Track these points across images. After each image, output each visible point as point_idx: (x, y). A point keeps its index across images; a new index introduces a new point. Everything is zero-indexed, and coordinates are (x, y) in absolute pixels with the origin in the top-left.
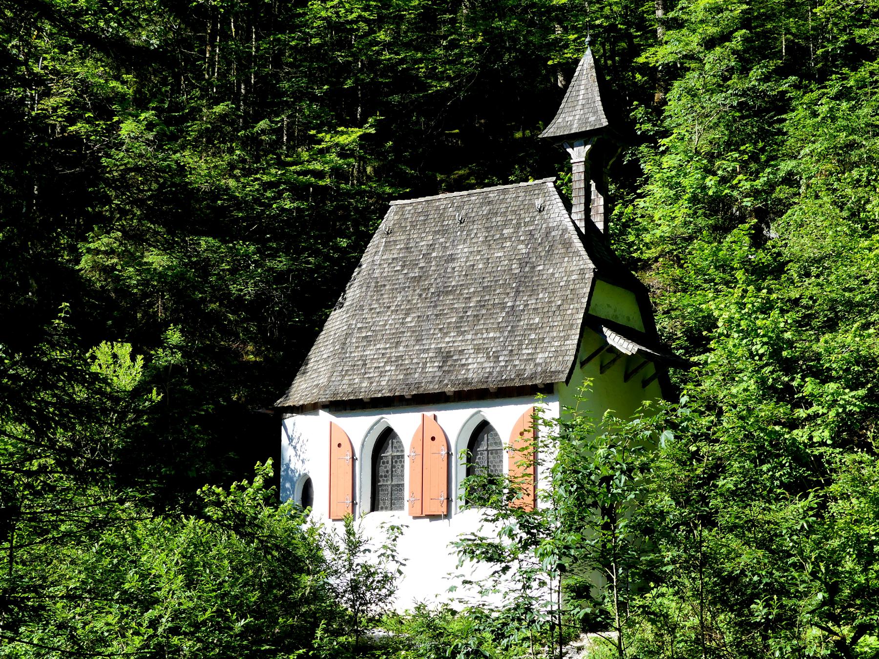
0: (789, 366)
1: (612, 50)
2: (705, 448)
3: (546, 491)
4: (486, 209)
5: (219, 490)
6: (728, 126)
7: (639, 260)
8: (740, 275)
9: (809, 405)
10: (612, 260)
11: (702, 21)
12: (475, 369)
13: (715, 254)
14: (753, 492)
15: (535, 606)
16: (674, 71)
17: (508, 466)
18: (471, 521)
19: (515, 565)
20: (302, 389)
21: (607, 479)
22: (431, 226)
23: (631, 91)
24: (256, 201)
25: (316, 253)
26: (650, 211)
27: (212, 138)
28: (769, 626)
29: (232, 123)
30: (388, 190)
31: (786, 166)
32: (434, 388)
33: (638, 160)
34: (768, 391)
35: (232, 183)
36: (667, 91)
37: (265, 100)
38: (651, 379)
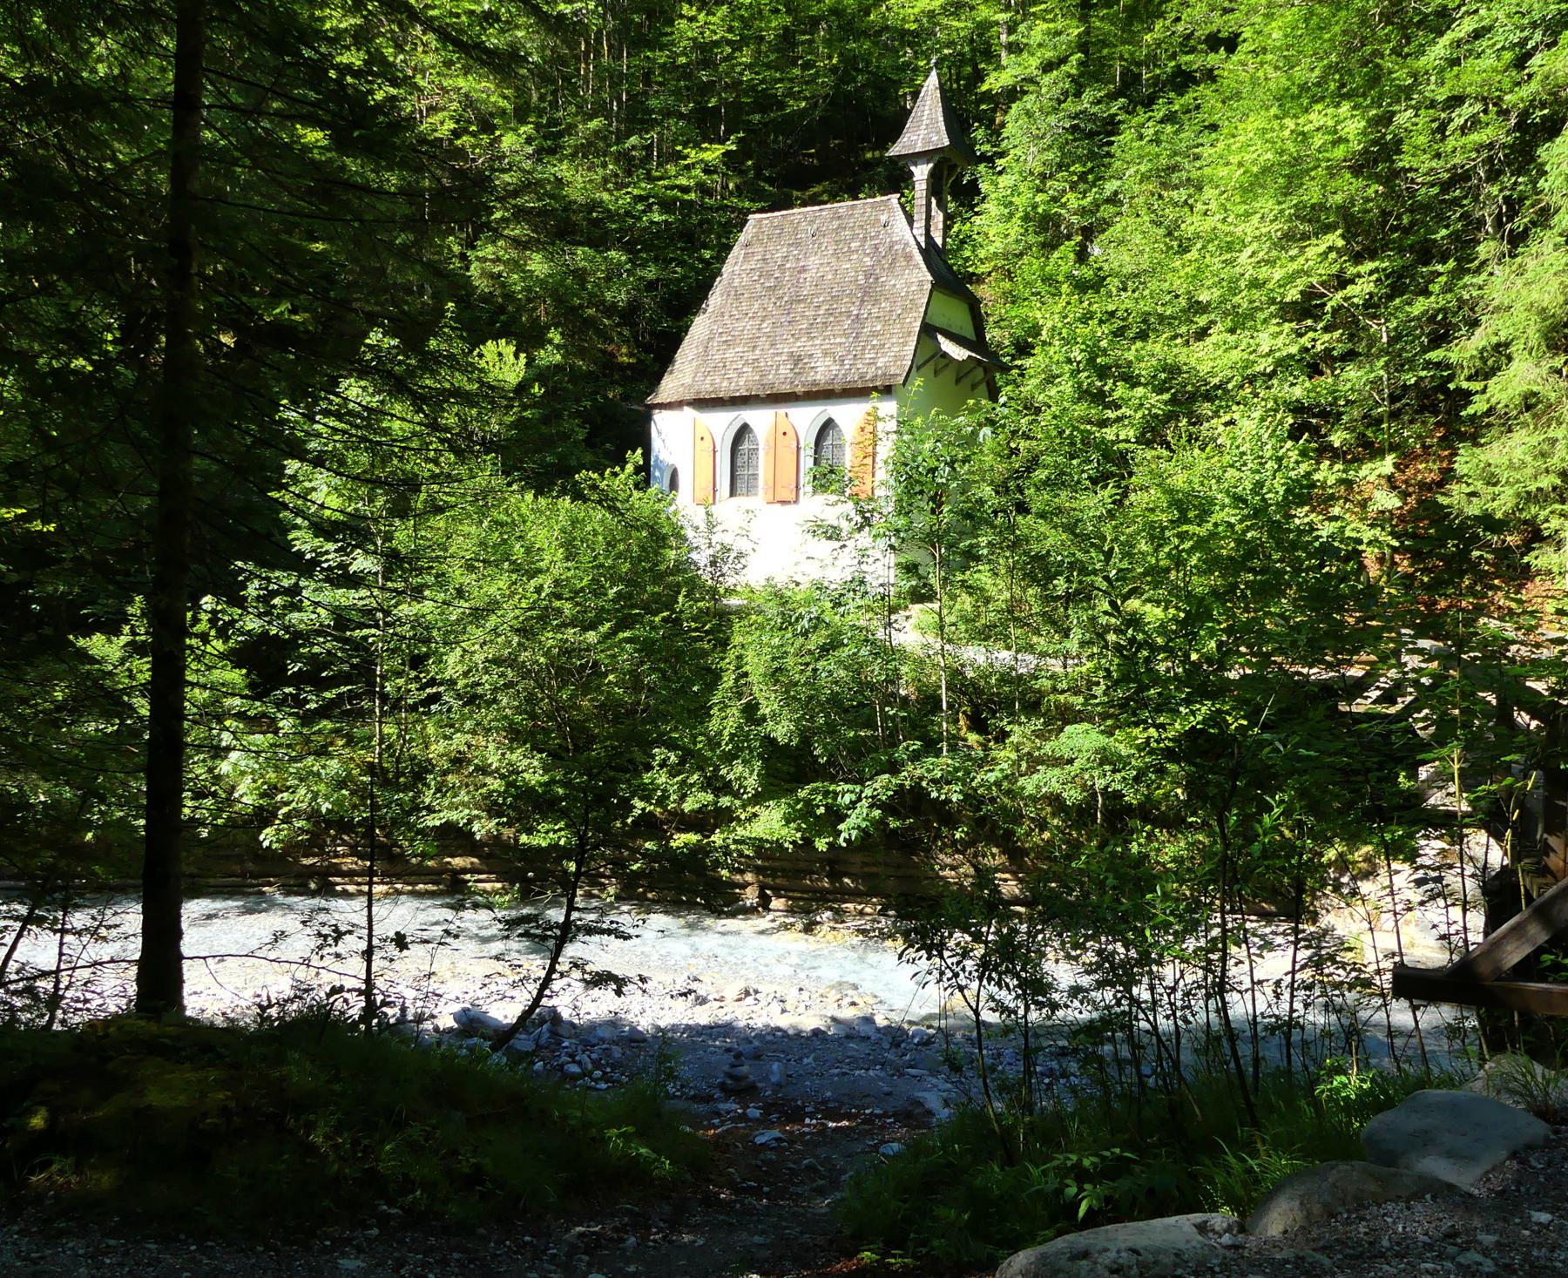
0: (1103, 372)
1: (958, 74)
2: (1023, 444)
3: (882, 485)
4: (835, 224)
5: (595, 476)
6: (1061, 149)
7: (974, 274)
8: (1065, 288)
9: (1118, 407)
10: (950, 276)
11: (1040, 45)
12: (823, 371)
13: (1042, 269)
14: (1063, 483)
15: (868, 578)
16: (1013, 94)
17: (849, 459)
18: (818, 506)
19: (850, 544)
20: (670, 387)
21: (933, 470)
22: (786, 239)
23: (970, 111)
24: (628, 213)
25: (681, 263)
26: (985, 229)
27: (589, 150)
28: (1068, 598)
29: (605, 138)
30: (747, 204)
31: (1110, 186)
32: (786, 388)
33: (976, 180)
34: (1083, 394)
35: (606, 196)
36: (1006, 112)
37: (636, 117)
38: (979, 383)
